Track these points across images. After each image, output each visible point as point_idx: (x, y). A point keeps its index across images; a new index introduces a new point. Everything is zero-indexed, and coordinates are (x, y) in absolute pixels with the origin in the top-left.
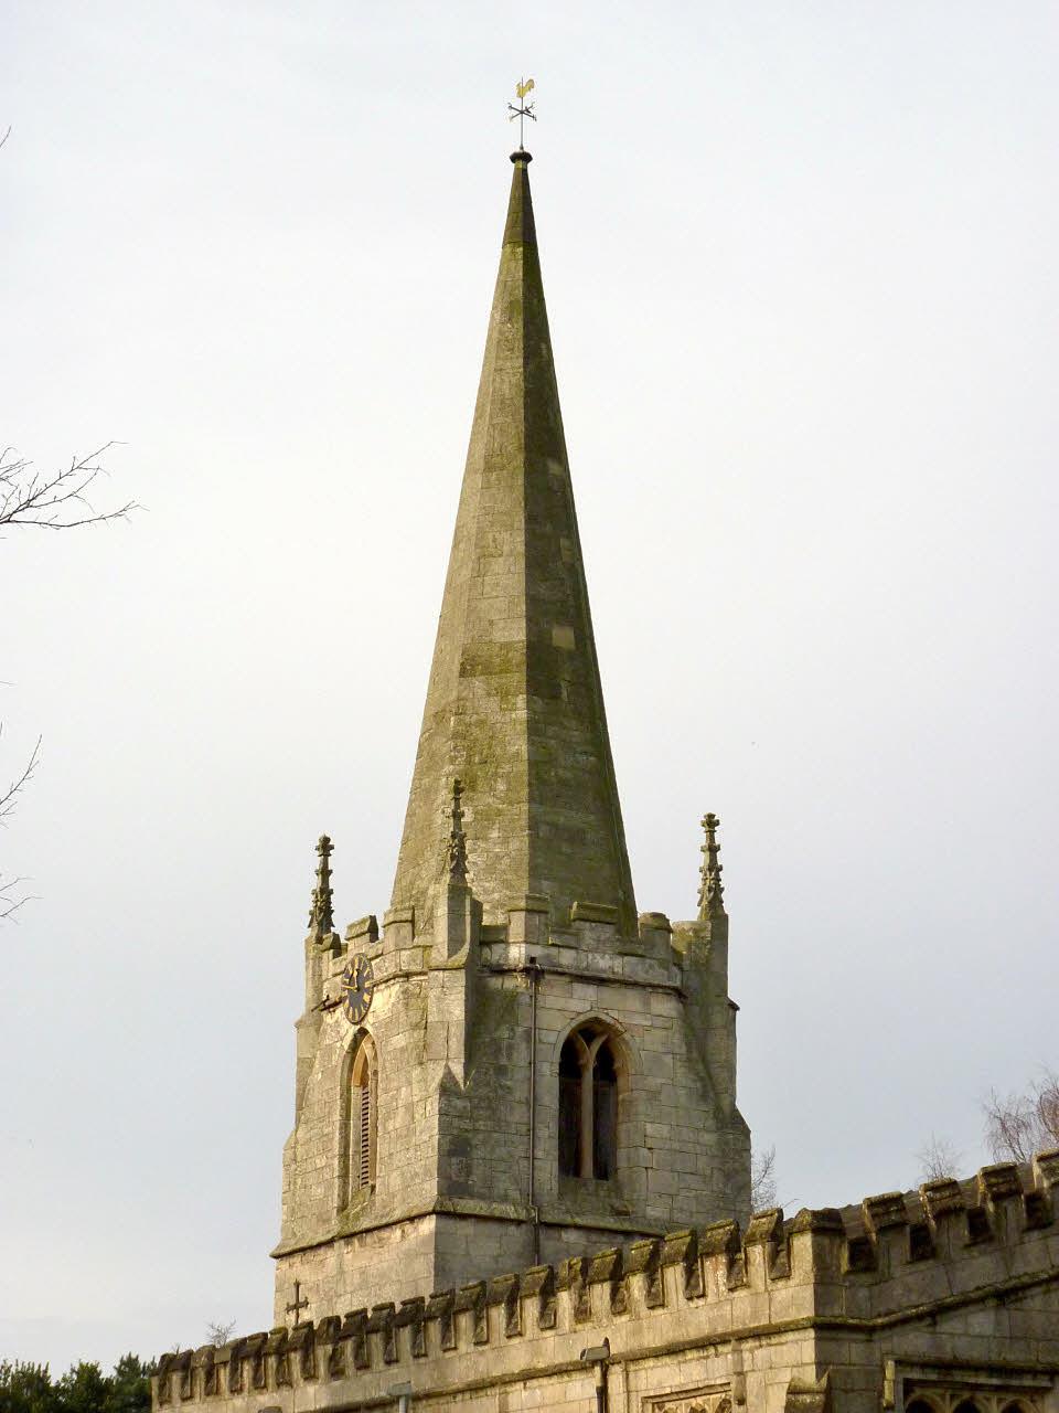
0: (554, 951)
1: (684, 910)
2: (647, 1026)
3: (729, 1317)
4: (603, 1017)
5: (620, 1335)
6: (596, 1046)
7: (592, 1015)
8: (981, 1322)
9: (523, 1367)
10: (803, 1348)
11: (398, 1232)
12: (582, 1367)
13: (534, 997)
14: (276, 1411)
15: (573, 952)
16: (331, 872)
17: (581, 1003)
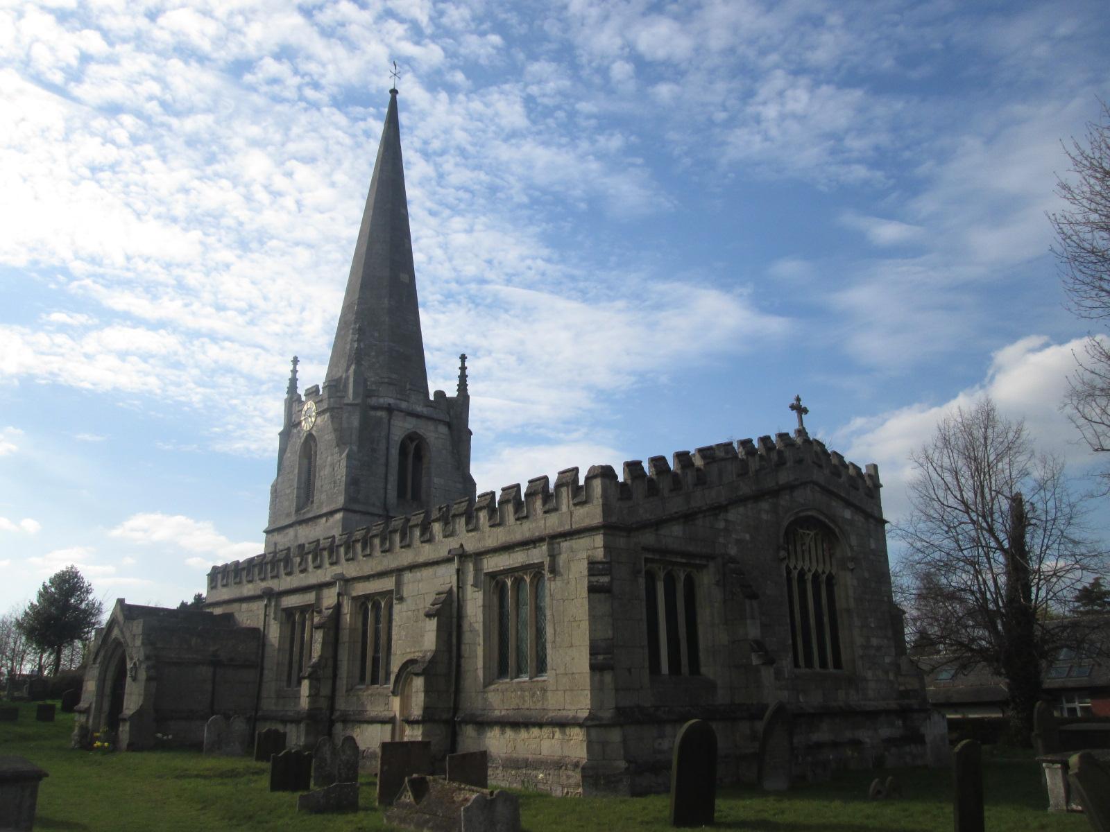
0: (398, 402)
1: (452, 392)
2: (435, 436)
3: (543, 527)
4: (418, 432)
5: (471, 543)
6: (415, 444)
7: (414, 430)
8: (677, 530)
9: (410, 561)
10: (599, 540)
11: (324, 519)
12: (448, 560)
13: (389, 421)
14: (327, 389)
15: (406, 403)
16: (299, 361)
17: (409, 425)
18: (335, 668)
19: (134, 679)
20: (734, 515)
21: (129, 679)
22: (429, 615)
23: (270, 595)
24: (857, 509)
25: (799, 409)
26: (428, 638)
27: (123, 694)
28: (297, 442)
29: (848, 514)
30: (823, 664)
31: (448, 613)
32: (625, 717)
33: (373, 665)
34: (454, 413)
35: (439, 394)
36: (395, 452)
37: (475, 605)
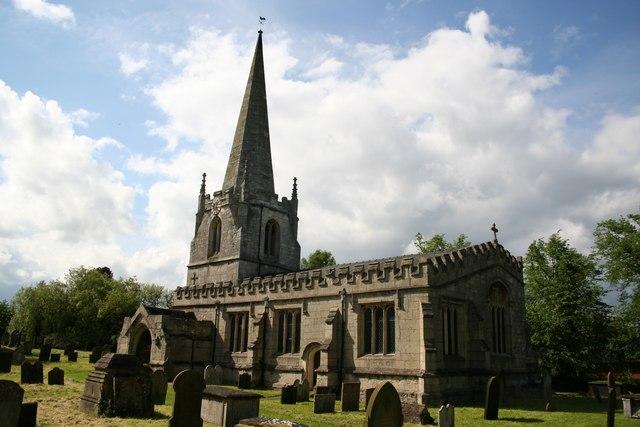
2: (282, 221)
18: (265, 344)
19: (158, 344)
20: (472, 281)
21: (153, 345)
22: (328, 323)
23: (218, 305)
24: (515, 277)
25: (495, 230)
26: (328, 332)
27: (149, 352)
28: (208, 220)
29: (511, 280)
30: (500, 351)
31: (338, 322)
32: (440, 373)
33: (290, 343)
34: (290, 207)
35: (284, 199)
36: (263, 229)
37: (353, 321)
